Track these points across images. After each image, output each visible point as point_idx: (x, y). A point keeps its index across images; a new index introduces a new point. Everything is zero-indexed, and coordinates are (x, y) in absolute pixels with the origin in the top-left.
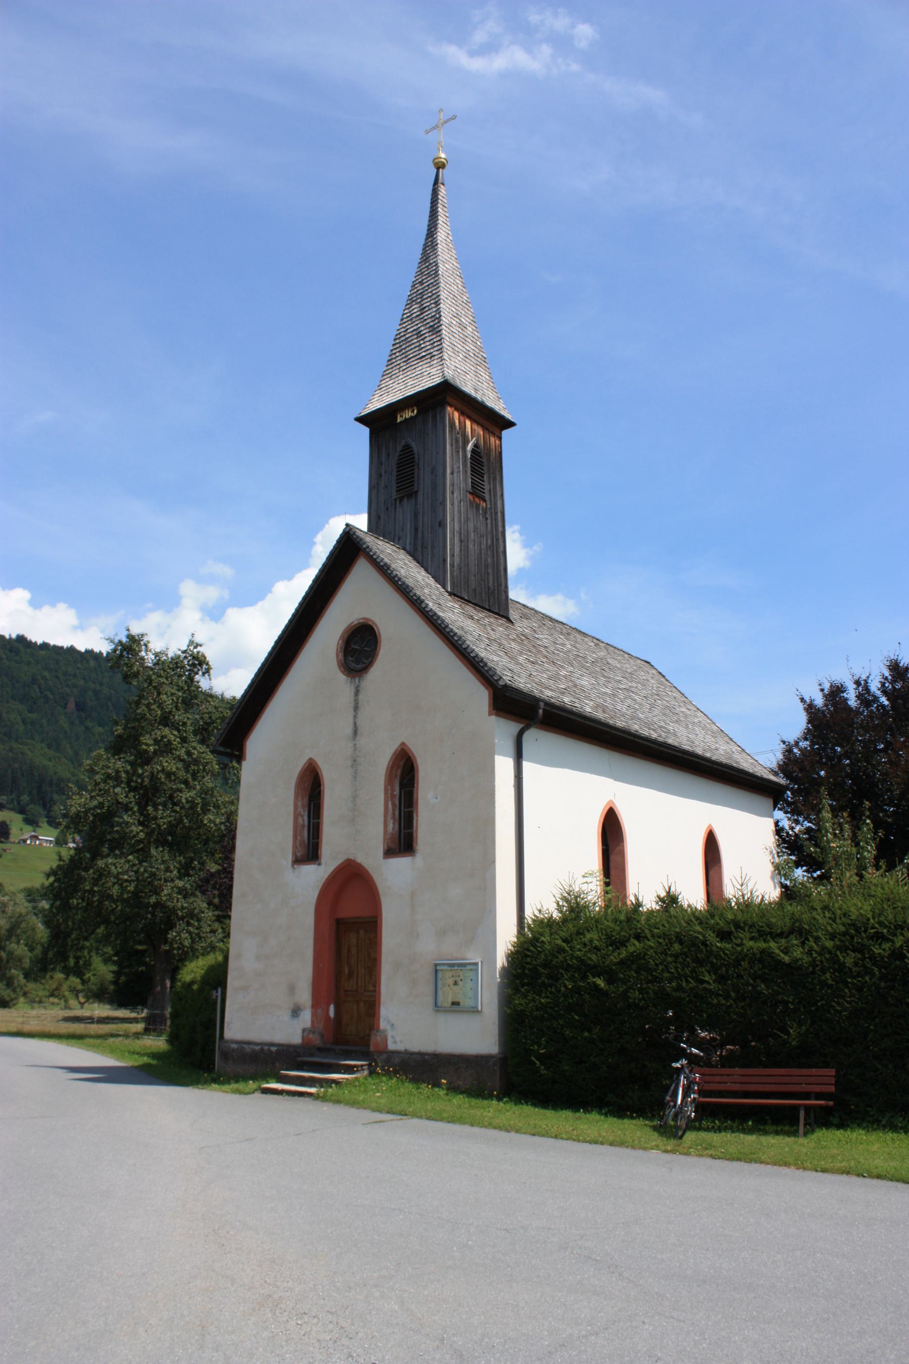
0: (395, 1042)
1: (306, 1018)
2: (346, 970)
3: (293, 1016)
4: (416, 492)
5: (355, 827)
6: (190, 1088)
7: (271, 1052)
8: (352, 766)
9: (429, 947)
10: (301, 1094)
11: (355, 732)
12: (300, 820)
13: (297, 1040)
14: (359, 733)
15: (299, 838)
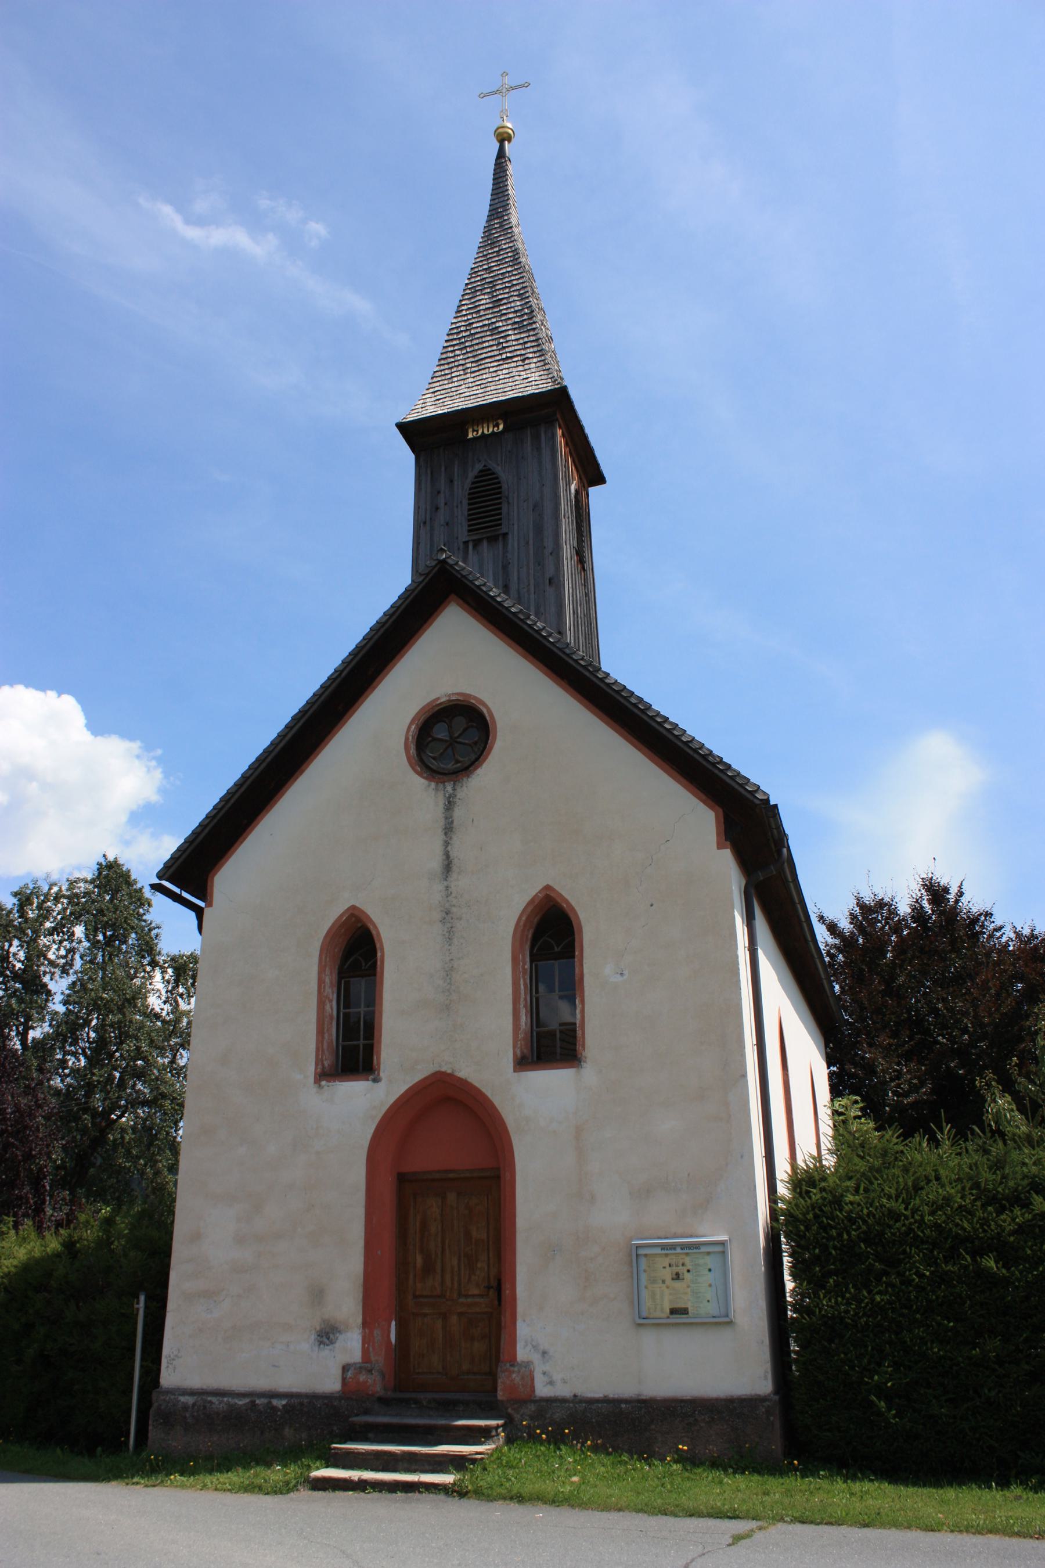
0: (551, 1383)
1: (351, 1346)
2: (419, 1260)
3: (321, 1343)
4: (505, 535)
5: (450, 1014)
6: (114, 1483)
7: (274, 1409)
8: (443, 921)
9: (614, 1217)
10: (361, 1486)
11: (448, 866)
12: (328, 1007)
13: (331, 1384)
14: (454, 868)
15: (326, 1036)
